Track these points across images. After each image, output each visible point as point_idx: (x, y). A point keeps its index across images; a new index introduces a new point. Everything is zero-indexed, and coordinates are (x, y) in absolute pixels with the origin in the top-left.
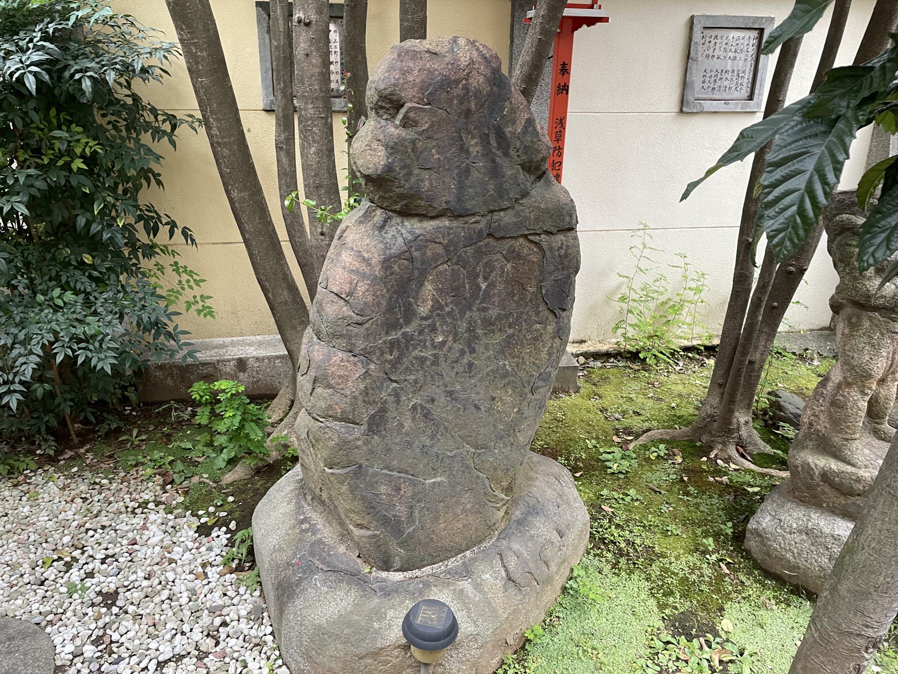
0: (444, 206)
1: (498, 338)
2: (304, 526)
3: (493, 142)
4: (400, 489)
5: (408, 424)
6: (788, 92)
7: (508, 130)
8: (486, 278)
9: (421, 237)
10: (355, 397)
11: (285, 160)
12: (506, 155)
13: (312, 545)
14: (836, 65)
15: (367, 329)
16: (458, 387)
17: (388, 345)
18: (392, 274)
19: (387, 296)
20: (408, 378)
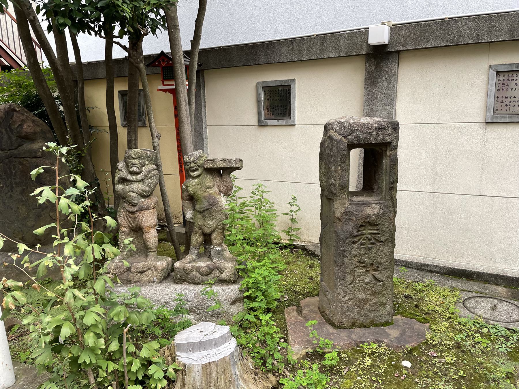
1: (19, 189)
3: (8, 130)
6: (89, 61)
7: (13, 127)
8: (14, 169)
12: (12, 134)
14: (128, 47)
16: (7, 201)
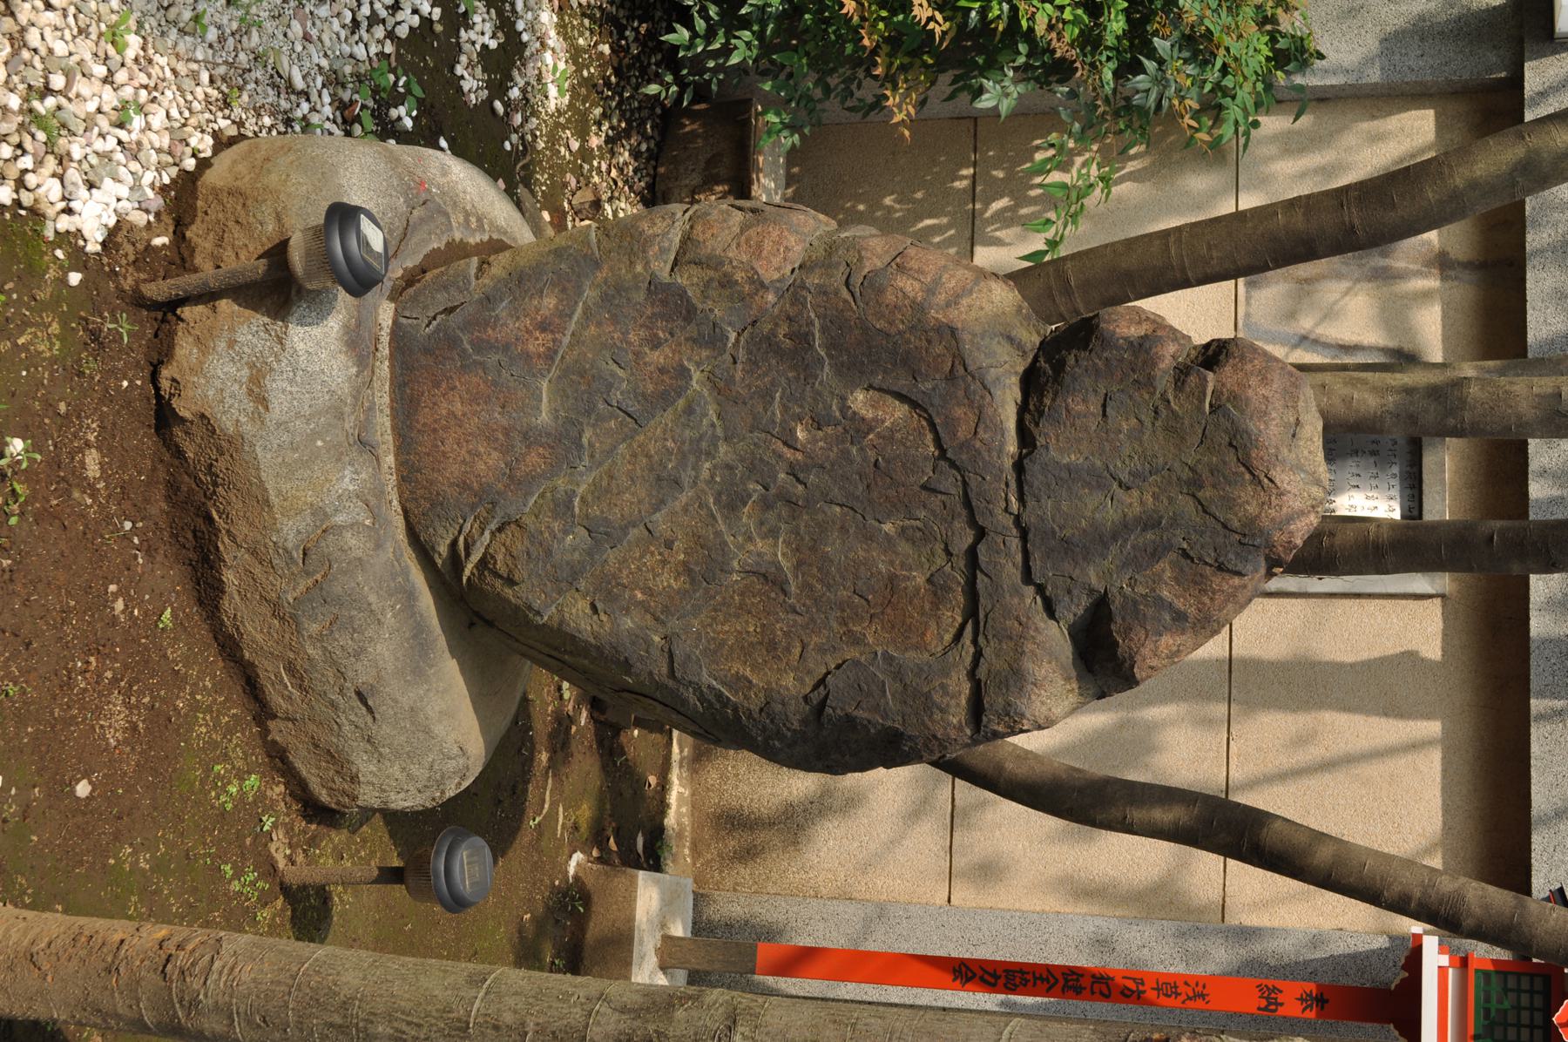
0: (1041, 441)
2: (473, 220)
4: (544, 330)
5: (656, 357)
9: (988, 398)
10: (722, 263)
11: (1162, 815)
13: (446, 215)
15: (836, 293)
17: (804, 329)
18: (929, 342)
19: (893, 331)
20: (739, 366)
